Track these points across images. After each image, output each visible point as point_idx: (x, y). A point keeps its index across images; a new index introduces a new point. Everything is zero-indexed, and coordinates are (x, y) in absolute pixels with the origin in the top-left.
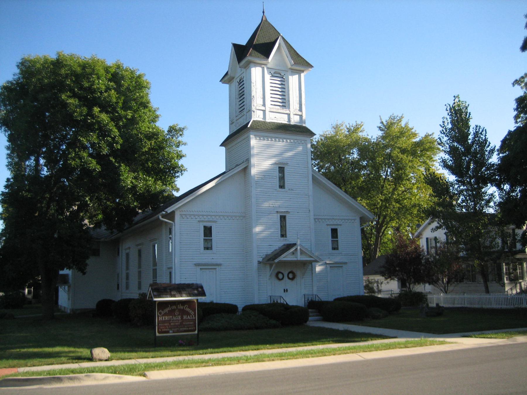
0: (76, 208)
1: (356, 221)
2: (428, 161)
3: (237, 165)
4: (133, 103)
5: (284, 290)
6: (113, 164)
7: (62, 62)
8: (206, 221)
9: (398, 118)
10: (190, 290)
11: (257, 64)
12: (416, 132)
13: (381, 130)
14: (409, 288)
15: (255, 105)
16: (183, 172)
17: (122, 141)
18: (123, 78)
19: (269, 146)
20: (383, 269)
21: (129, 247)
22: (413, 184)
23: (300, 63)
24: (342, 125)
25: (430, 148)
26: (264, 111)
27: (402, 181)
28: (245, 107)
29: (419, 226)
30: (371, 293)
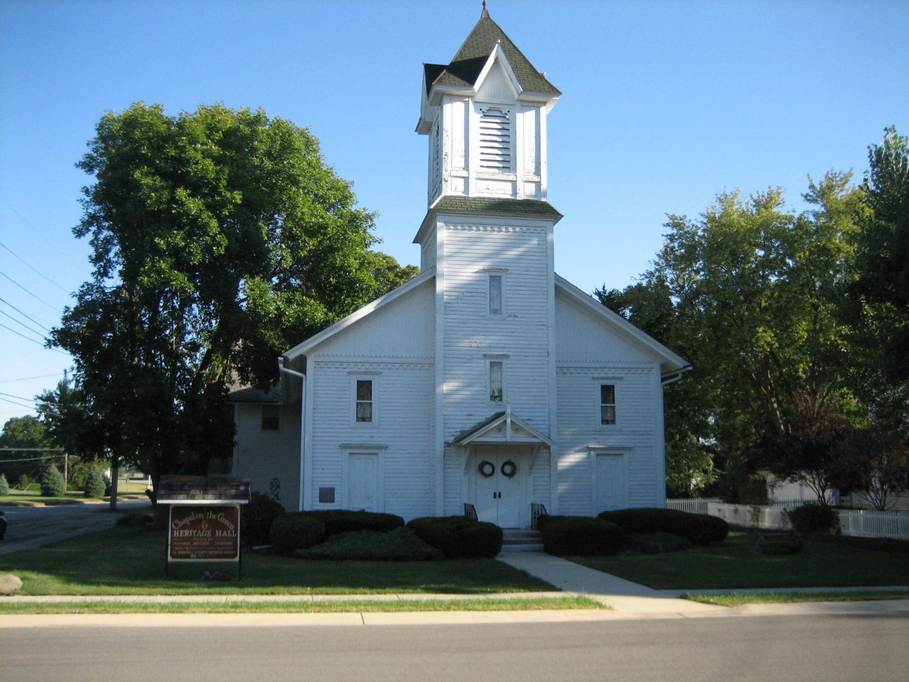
1: (653, 371)
5: (495, 494)
8: (362, 373)
9: (842, 176)
11: (454, 98)
13: (808, 200)
15: (449, 168)
19: (474, 241)
26: (466, 179)
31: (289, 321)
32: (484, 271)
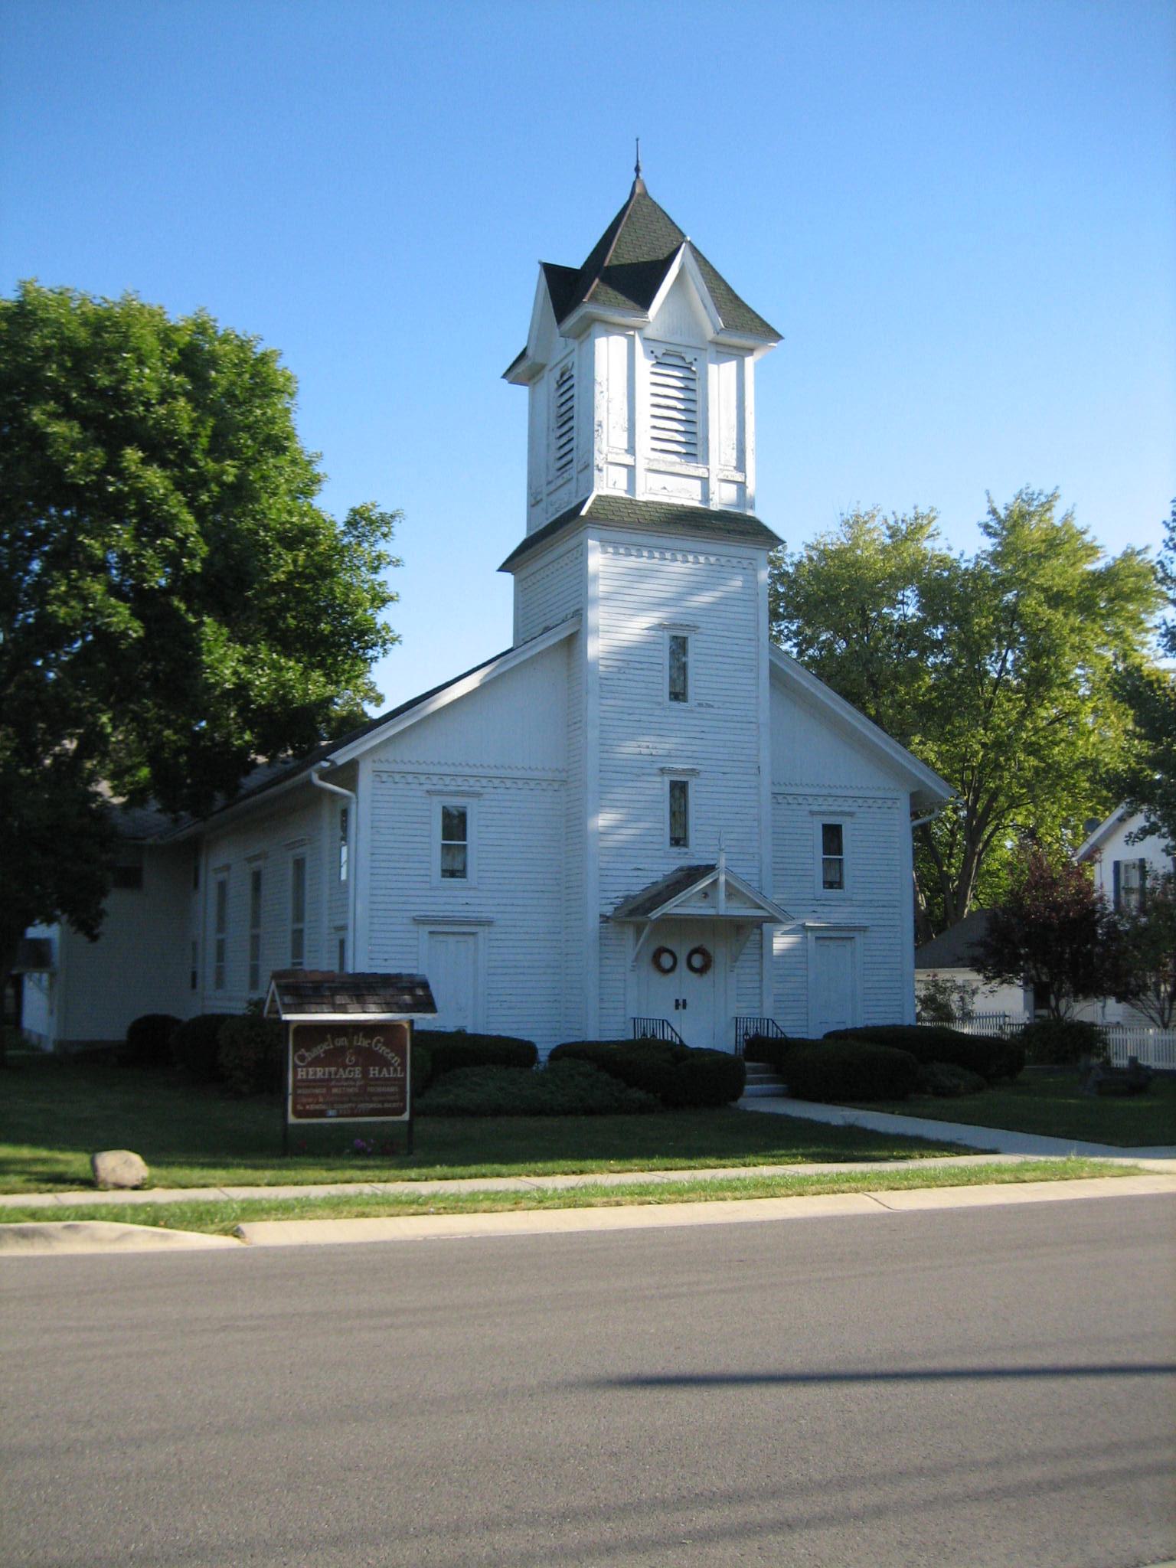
0: (70, 745)
2: (1129, 631)
3: (547, 629)
4: (244, 438)
5: (684, 1007)
6: (181, 619)
7: (33, 313)
9: (1043, 499)
10: (391, 991)
12: (1096, 543)
13: (989, 534)
14: (1057, 1009)
15: (605, 449)
16: (388, 646)
17: (206, 549)
18: (213, 362)
19: (642, 575)
20: (979, 951)
21: (227, 863)
22: (1083, 700)
23: (744, 327)
24: (873, 516)
25: (1138, 591)
26: (631, 469)
27: (1049, 689)
28: (574, 454)
29: (1092, 825)
30: (942, 1020)
31: (263, 697)
32: (660, 627)
